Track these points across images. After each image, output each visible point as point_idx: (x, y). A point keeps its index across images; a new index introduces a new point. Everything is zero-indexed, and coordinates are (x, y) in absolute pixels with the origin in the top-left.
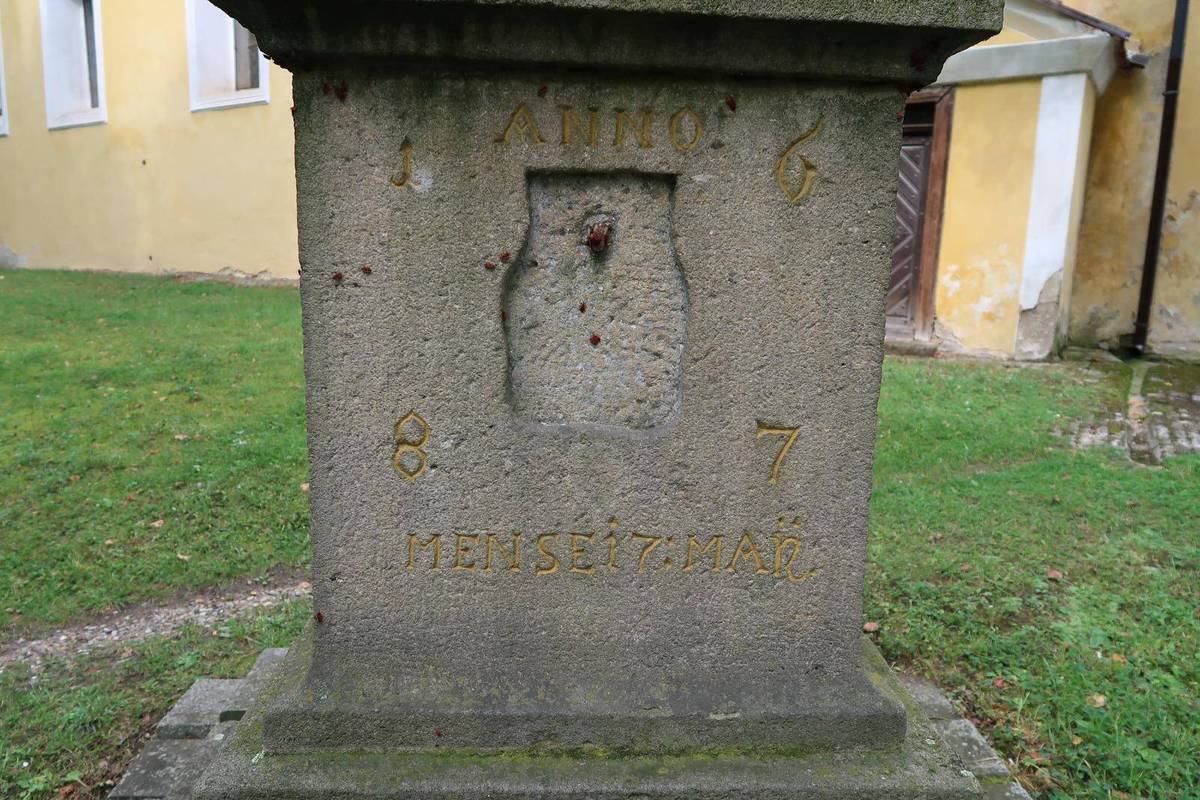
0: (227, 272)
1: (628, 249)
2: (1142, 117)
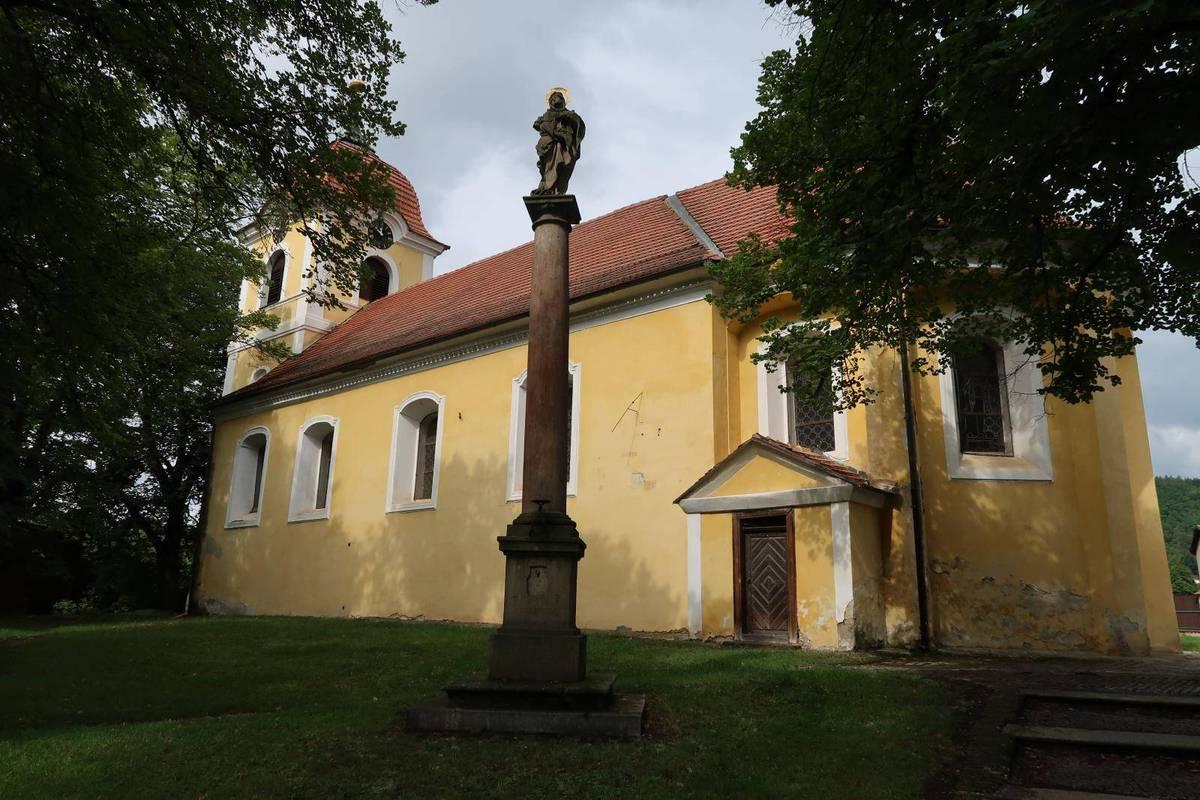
0: (395, 617)
1: (541, 575)
2: (900, 527)
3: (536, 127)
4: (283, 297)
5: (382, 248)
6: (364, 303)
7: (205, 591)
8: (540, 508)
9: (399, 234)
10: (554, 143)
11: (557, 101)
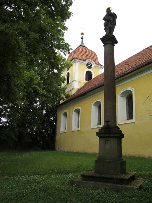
3: (103, 19)
4: (70, 82)
5: (90, 69)
6: (87, 81)
7: (57, 148)
8: (107, 124)
9: (93, 65)
10: (108, 22)
11: (108, 10)
